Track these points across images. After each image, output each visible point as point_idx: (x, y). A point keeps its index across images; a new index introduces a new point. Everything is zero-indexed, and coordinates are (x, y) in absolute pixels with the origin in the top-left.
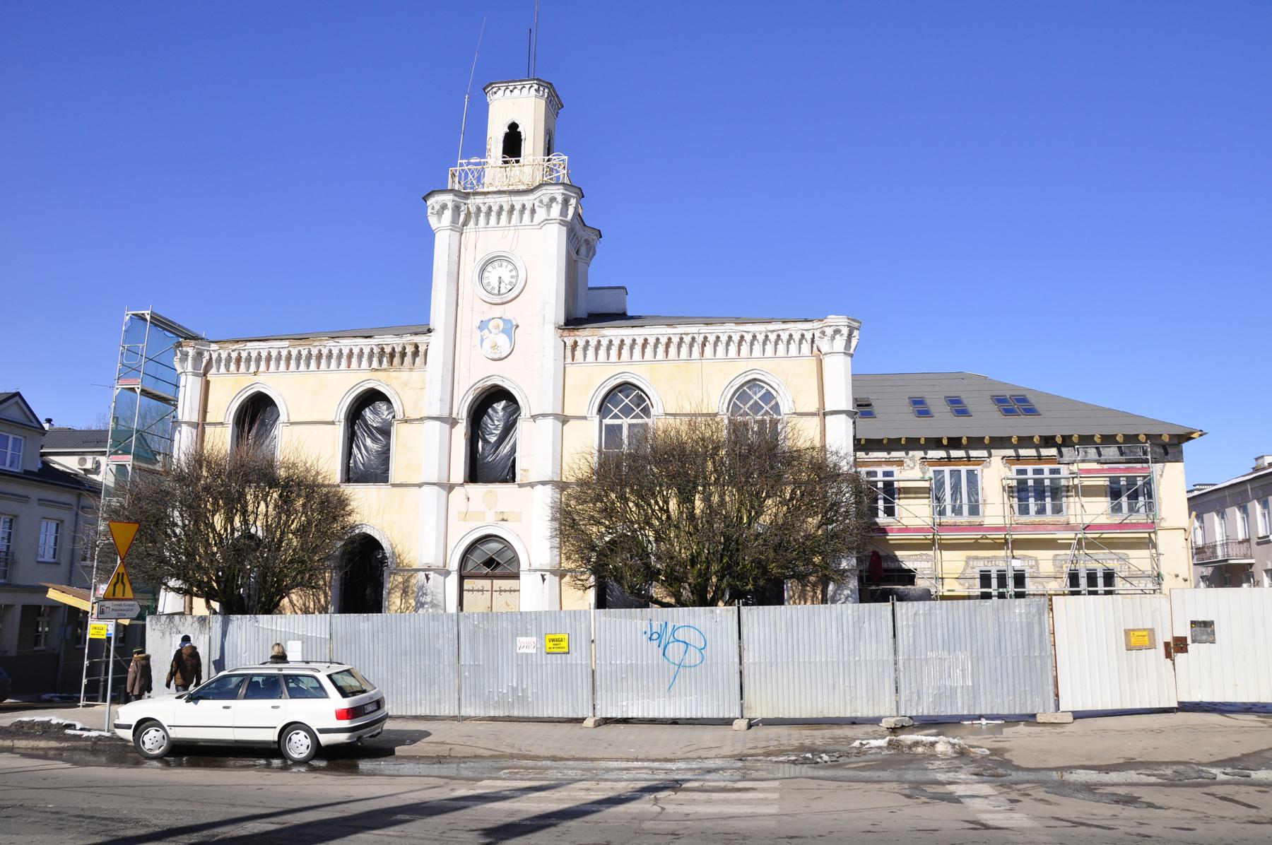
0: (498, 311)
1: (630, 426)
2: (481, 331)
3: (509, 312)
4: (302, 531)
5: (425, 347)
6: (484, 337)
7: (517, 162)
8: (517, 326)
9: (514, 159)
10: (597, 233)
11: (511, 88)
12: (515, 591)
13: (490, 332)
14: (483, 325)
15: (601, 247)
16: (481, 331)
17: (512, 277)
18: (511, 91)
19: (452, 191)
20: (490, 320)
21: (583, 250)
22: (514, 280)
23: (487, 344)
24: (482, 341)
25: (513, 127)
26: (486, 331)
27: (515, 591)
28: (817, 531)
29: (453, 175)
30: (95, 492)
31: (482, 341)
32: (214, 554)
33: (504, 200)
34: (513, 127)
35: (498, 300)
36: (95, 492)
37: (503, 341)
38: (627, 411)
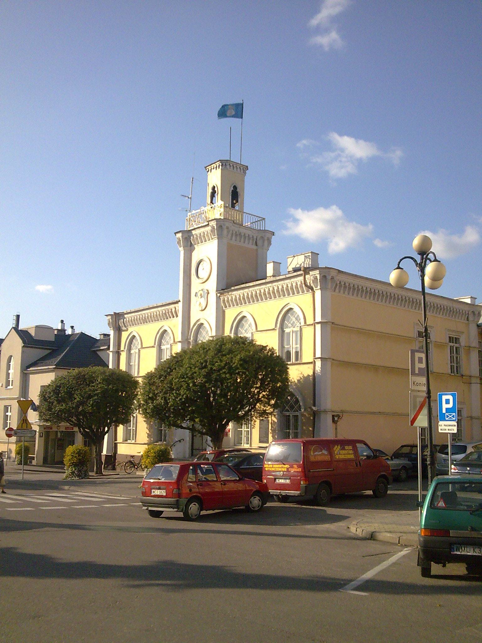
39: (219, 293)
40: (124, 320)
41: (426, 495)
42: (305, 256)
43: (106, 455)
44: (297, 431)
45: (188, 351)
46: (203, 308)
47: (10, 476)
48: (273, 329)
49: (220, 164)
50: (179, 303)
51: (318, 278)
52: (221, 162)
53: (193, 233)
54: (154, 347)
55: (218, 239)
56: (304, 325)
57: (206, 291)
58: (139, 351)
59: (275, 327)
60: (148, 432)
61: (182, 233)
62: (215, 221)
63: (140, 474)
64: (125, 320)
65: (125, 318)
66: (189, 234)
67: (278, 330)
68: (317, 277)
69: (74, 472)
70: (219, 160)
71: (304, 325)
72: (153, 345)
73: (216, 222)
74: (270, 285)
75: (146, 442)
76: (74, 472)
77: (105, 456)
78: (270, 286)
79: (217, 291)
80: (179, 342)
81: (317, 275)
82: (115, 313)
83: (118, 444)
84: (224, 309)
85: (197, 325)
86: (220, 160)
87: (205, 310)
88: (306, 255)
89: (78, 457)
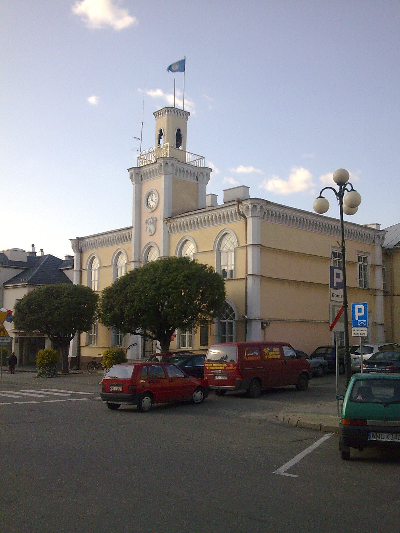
11: (159, 113)
70: (165, 107)
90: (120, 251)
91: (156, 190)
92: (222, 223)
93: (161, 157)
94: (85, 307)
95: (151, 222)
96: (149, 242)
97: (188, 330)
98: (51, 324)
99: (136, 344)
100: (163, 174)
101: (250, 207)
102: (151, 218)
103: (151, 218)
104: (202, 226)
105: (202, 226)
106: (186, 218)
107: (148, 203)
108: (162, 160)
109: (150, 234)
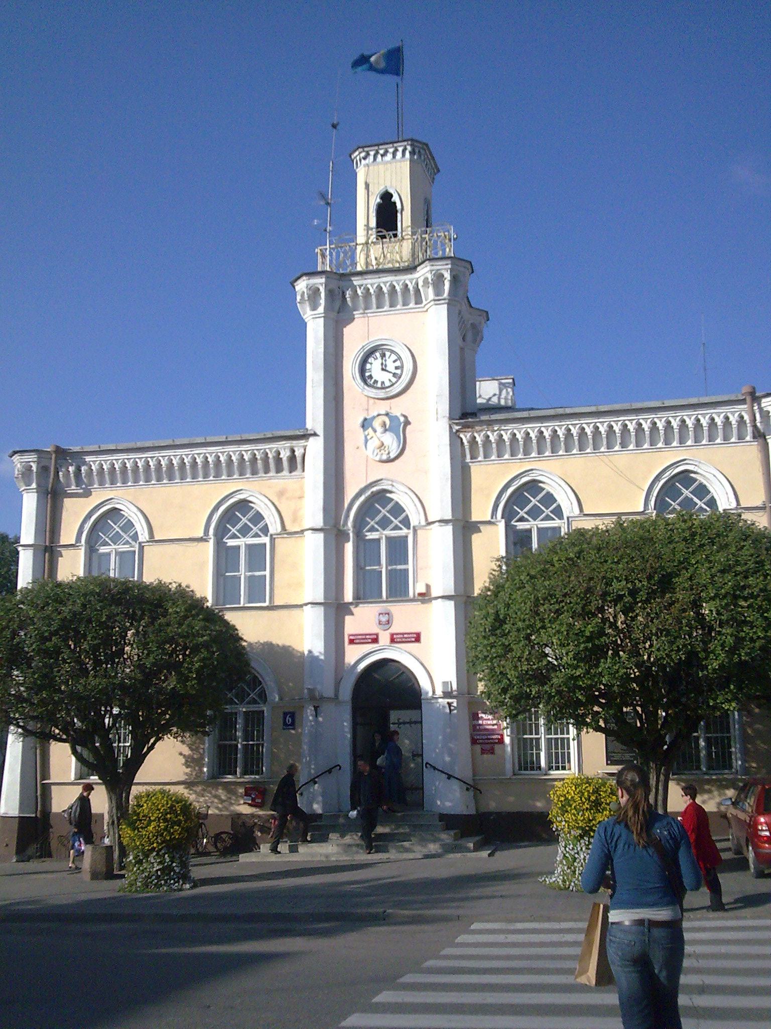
0: (383, 407)
1: (540, 530)
2: (364, 430)
3: (398, 408)
4: (31, 655)
5: (302, 451)
6: (369, 437)
7: (395, 236)
8: (407, 423)
9: (391, 233)
10: (485, 314)
11: (382, 152)
12: (416, 722)
13: (375, 431)
14: (366, 424)
15: (488, 331)
16: (364, 430)
17: (397, 368)
18: (382, 156)
19: (323, 272)
20: (374, 418)
21: (469, 336)
22: (399, 372)
23: (373, 444)
24: (366, 441)
25: (386, 197)
26: (370, 430)
27: (416, 722)
28: (68, 659)
29: (323, 256)
30: (724, 762)
31: (366, 441)
32: (71, 645)
33: (385, 281)
34: (386, 197)
35: (382, 395)
36: (724, 762)
37: (390, 440)
38: (535, 513)
39: (457, 424)
40: (78, 470)
41: (50, 855)
42: (500, 384)
43: (19, 817)
44: (728, 735)
45: (661, 534)
46: (392, 456)
47: (458, 907)
48: (201, 540)
49: (409, 148)
50: (311, 439)
51: (34, 468)
52: (411, 145)
53: (355, 283)
54: (206, 541)
55: (448, 304)
56: (148, 542)
57: (402, 419)
58: (141, 548)
59: (77, 542)
60: (186, 751)
61: (327, 278)
62: (449, 262)
63: (247, 860)
64: (84, 469)
65: (85, 463)
66: (342, 284)
67: (83, 548)
68: (31, 467)
69: (169, 868)
70: (410, 137)
71: (148, 542)
72: (201, 534)
73: (452, 264)
74: (186, 451)
75: (183, 778)
76: (169, 868)
77: (17, 819)
78: (93, 461)
79: (451, 418)
80: (315, 530)
81: (32, 464)
82: (58, 448)
83: (53, 787)
84: (468, 459)
85: (369, 493)
86: (412, 140)
87: (397, 461)
88: (503, 381)
89: (186, 822)
90: (242, 497)
91: (406, 346)
92: (673, 445)
93: (440, 254)
94: (650, 659)
95: (384, 424)
96: (379, 478)
97: (120, 712)
98: (87, 729)
99: (339, 767)
100: (443, 302)
101: (34, 468)
102: (387, 414)
103: (387, 414)
104: (499, 455)
105: (499, 455)
106: (580, 420)
107: (367, 374)
108: (447, 264)
109: (385, 457)
